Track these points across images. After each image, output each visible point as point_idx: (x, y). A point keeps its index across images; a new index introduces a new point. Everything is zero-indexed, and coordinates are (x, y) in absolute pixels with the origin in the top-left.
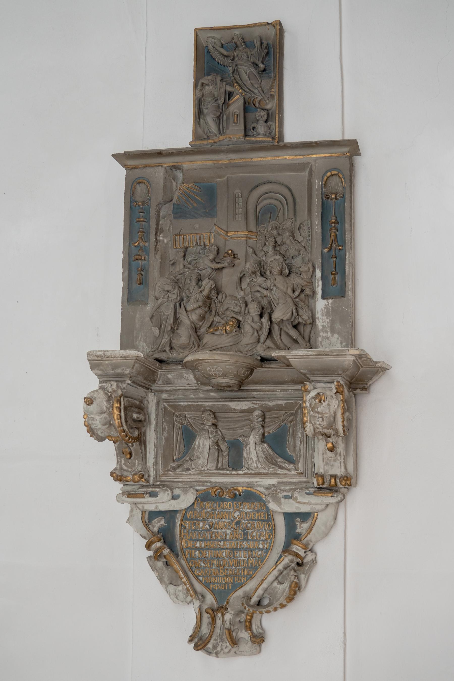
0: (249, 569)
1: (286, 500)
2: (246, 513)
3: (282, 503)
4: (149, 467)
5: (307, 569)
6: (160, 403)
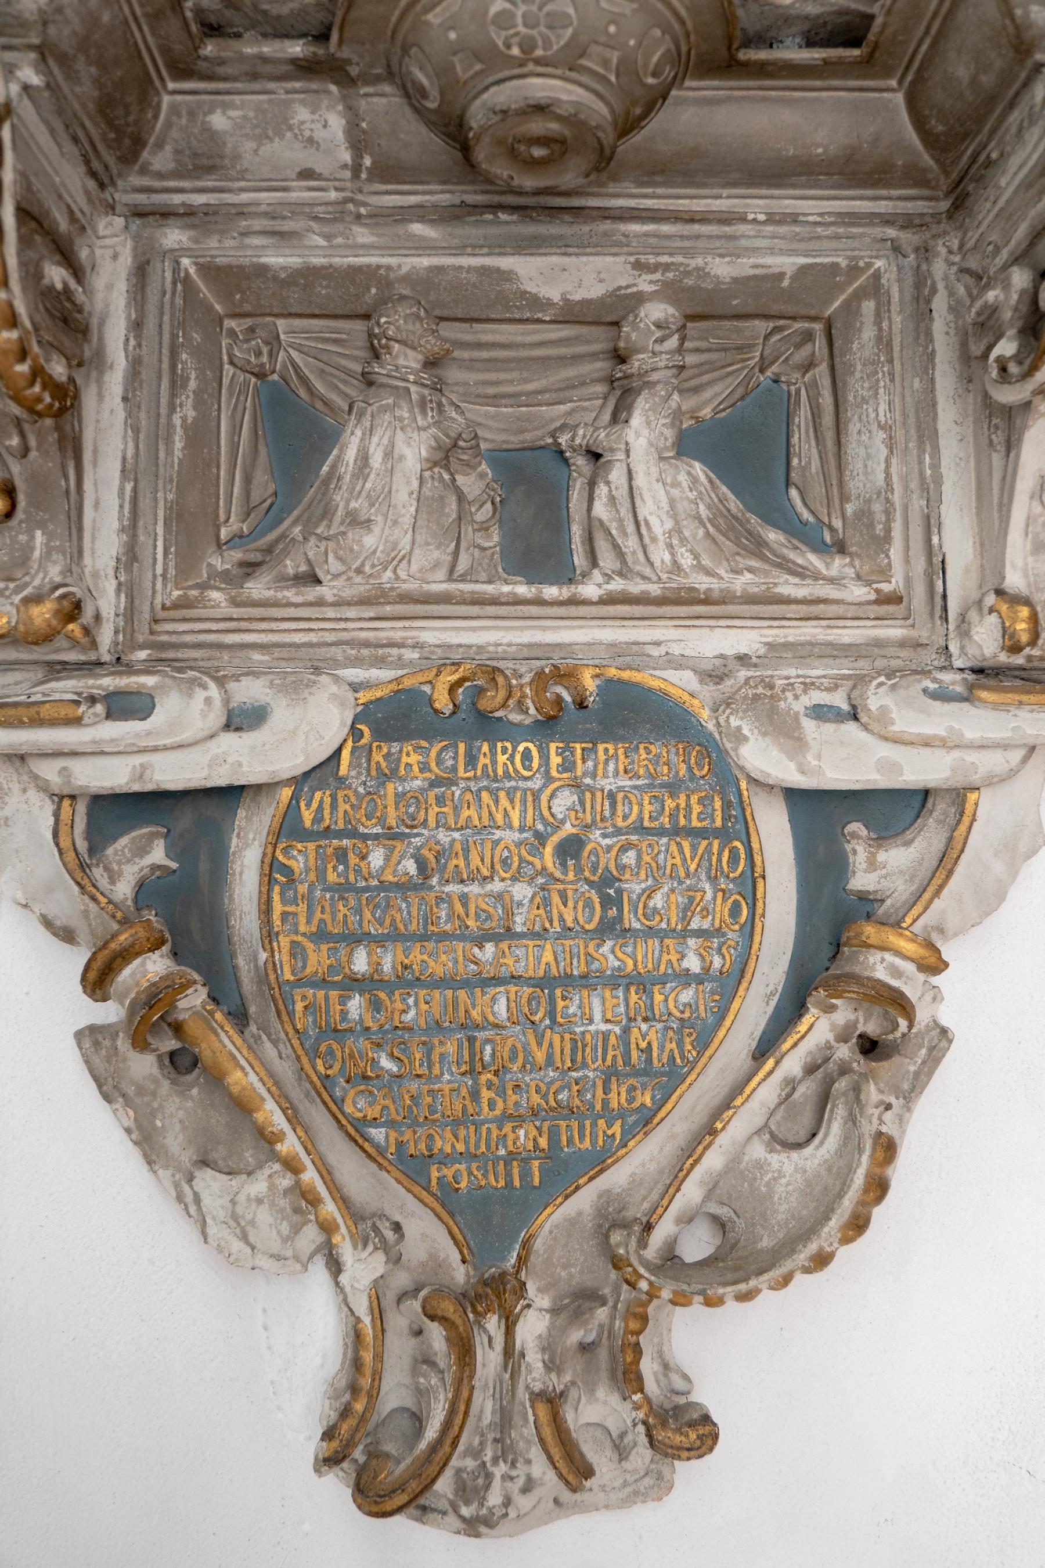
0: (632, 1081)
1: (829, 728)
2: (612, 796)
3: (809, 739)
4: (96, 575)
5: (912, 1068)
6: (149, 269)
